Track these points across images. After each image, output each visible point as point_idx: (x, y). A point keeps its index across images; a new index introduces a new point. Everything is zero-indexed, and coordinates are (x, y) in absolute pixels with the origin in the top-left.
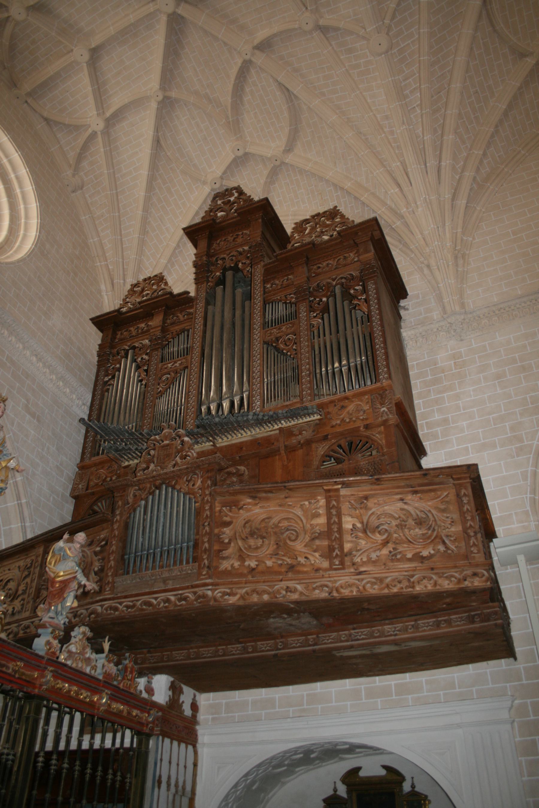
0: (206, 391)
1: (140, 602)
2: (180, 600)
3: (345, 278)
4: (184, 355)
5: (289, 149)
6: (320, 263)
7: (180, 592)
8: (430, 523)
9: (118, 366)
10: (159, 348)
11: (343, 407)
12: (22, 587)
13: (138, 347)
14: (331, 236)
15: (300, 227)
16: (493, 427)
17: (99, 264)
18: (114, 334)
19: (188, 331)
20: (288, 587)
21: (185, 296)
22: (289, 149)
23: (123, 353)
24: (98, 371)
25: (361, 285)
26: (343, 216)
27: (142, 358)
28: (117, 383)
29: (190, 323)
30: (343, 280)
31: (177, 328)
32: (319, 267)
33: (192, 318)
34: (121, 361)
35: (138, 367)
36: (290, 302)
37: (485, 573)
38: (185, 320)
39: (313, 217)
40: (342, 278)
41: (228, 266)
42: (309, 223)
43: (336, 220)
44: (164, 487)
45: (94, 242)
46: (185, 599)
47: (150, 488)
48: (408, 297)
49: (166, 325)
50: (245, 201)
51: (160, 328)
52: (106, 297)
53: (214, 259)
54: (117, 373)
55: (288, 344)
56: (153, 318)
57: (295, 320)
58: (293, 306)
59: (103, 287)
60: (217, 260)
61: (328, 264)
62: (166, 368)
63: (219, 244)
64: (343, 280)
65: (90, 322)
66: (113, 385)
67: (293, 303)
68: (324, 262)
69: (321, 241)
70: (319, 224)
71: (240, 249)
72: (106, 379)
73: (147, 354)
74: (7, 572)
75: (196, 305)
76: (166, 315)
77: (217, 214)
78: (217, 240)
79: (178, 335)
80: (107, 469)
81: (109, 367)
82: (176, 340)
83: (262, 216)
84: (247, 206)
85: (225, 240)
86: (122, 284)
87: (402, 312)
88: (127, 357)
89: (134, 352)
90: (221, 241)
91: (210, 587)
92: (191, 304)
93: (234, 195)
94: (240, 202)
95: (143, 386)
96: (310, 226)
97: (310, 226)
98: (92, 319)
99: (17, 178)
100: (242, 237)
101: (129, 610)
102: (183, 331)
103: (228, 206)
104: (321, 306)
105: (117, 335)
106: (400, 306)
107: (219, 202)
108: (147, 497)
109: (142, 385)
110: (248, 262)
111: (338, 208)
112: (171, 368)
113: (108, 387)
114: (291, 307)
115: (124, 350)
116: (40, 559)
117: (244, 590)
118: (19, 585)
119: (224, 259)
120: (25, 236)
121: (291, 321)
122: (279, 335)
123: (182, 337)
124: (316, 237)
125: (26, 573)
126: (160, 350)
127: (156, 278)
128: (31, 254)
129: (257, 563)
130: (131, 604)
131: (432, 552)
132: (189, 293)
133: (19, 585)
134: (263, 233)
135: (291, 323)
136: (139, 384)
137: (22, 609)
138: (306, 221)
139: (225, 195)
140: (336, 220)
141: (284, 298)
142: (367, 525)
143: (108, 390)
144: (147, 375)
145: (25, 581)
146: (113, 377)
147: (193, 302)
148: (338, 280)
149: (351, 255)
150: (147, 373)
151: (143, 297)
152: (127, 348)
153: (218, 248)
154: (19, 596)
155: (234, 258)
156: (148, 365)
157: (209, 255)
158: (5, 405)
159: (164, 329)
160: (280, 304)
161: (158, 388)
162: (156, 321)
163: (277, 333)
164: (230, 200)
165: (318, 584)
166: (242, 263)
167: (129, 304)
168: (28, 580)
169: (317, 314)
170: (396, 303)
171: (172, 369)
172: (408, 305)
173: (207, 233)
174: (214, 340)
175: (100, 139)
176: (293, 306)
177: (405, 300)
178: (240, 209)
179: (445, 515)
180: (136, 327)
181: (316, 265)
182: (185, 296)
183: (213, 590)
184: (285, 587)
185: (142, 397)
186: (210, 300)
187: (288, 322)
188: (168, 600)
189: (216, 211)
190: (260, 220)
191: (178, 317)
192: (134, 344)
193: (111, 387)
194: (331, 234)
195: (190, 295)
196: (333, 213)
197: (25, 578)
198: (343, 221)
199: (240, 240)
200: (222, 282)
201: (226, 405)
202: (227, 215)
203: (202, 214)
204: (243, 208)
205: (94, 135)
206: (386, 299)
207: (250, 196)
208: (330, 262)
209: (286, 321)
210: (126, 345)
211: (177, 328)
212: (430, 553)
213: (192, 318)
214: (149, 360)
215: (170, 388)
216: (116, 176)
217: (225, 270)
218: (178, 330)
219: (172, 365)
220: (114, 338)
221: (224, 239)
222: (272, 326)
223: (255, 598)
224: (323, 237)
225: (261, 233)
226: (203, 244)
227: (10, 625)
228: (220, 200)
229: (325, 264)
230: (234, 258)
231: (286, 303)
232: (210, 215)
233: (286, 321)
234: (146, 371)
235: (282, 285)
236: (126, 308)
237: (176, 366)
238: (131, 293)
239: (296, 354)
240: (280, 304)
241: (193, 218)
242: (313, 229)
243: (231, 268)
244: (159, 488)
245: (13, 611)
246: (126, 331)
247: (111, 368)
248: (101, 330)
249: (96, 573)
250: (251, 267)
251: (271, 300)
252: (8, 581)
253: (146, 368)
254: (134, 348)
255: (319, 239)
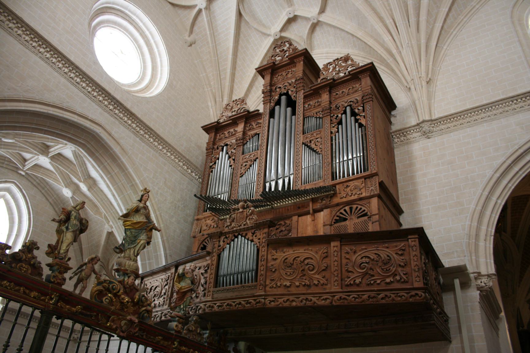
0: (269, 173)
1: (226, 304)
2: (247, 304)
3: (353, 102)
4: (256, 150)
5: (322, 11)
6: (337, 91)
7: (247, 299)
8: (392, 263)
9: (218, 156)
10: (241, 145)
11: (347, 186)
12: (164, 291)
13: (229, 145)
14: (345, 74)
15: (326, 66)
16: (446, 195)
17: (206, 90)
18: (216, 135)
19: (258, 134)
20: (307, 299)
21: (257, 112)
22: (322, 11)
23: (220, 148)
24: (207, 159)
25: (362, 107)
26: (352, 60)
27: (231, 152)
28: (218, 167)
29: (260, 130)
30: (351, 103)
31: (252, 132)
32: (337, 94)
33: (261, 126)
34: (220, 153)
35: (229, 157)
36: (319, 117)
37: (423, 294)
38: (257, 127)
39: (334, 61)
40: (351, 102)
41: (283, 92)
42: (331, 65)
43: (348, 63)
44: (240, 237)
45: (203, 76)
46: (250, 303)
47: (232, 237)
48: (397, 108)
49: (246, 130)
50: (293, 50)
51: (242, 133)
52: (211, 110)
53: (274, 88)
54: (217, 161)
55: (317, 144)
56: (238, 126)
57: (322, 129)
58: (321, 119)
59: (210, 104)
60: (276, 89)
61: (343, 92)
62: (245, 158)
63: (277, 78)
64: (351, 103)
65: (201, 129)
66: (215, 168)
67: (321, 118)
68: (340, 90)
69: (339, 77)
70: (338, 66)
71: (290, 82)
72: (211, 164)
73: (234, 149)
74: (156, 281)
75: (264, 118)
76: (246, 123)
77: (276, 58)
78: (276, 75)
79: (253, 137)
80: (211, 220)
81: (213, 157)
82: (252, 140)
83: (303, 60)
84: (294, 54)
85: (281, 75)
86: (221, 101)
87: (392, 119)
88: (223, 151)
89: (227, 148)
90: (278, 76)
91: (263, 297)
92: (260, 117)
93: (286, 46)
94: (290, 51)
95: (232, 170)
96: (332, 67)
97: (332, 67)
98: (202, 127)
99: (155, 42)
100: (291, 73)
101: (220, 308)
102: (256, 134)
103: (283, 52)
104: (338, 121)
105: (217, 136)
106: (392, 115)
107: (278, 51)
108: (230, 243)
109: (231, 168)
110: (294, 90)
111: (349, 55)
112: (248, 158)
113: (212, 169)
114: (320, 120)
115: (221, 146)
116: (173, 275)
117: (283, 299)
118: (162, 290)
119: (280, 88)
120: (161, 78)
121: (319, 130)
122: (312, 139)
123: (255, 138)
124: (335, 74)
125: (166, 283)
126: (242, 147)
127: (239, 100)
128: (165, 89)
129: (290, 283)
130: (221, 304)
131: (392, 280)
132: (258, 110)
133: (162, 290)
134: (303, 71)
135: (319, 131)
136: (230, 168)
137: (164, 303)
138: (330, 64)
139: (281, 46)
140: (348, 63)
141: (315, 114)
142: (354, 262)
143: (212, 172)
144: (234, 162)
145: (166, 287)
146: (215, 163)
147: (261, 116)
148: (348, 103)
149: (357, 85)
150: (234, 161)
151: (232, 113)
152: (223, 145)
153: (276, 81)
154: (162, 296)
155: (286, 87)
156: (235, 156)
157: (271, 85)
158: (149, 195)
159: (244, 133)
160: (313, 118)
161: (241, 171)
162: (240, 128)
163: (311, 137)
164: (284, 49)
165: (324, 297)
166: (291, 91)
167: (224, 117)
168: (167, 287)
169: (335, 125)
170: (387, 113)
171: (249, 159)
172: (397, 114)
173: (270, 71)
174: (274, 141)
175: (204, 12)
176: (321, 119)
177: (395, 111)
178: (290, 55)
179: (401, 258)
180: (228, 131)
181: (335, 92)
182: (257, 112)
183: (265, 299)
184: (305, 298)
185: (231, 177)
186: (272, 114)
187: (317, 130)
188: (240, 304)
189: (275, 57)
190: (302, 62)
191: (252, 125)
192: (227, 143)
193: (214, 170)
194: (345, 72)
195: (260, 111)
196: (346, 59)
197: (165, 286)
198: (353, 63)
199: (289, 75)
200: (278, 103)
201: (280, 182)
202: (282, 59)
203: (268, 58)
204: (292, 54)
205: (200, 11)
206: (379, 113)
207: (296, 46)
208: (344, 90)
209: (317, 130)
210: (222, 143)
211: (252, 132)
212: (390, 280)
213: (261, 126)
214: (235, 153)
215: (247, 171)
216: (215, 34)
217: (281, 95)
218: (253, 134)
219: (249, 156)
220: (215, 138)
221: (280, 74)
222: (308, 133)
223: (287, 304)
224: (340, 74)
225: (302, 71)
226: (268, 78)
227: (157, 312)
228: (278, 49)
229: (341, 92)
230: (286, 87)
231: (317, 118)
232: (272, 59)
233: (317, 130)
234: (234, 160)
235: (314, 105)
236: (223, 119)
237: (251, 157)
238: (225, 109)
239: (321, 151)
240: (313, 118)
241: (262, 62)
242: (334, 68)
243: (284, 94)
244: (237, 237)
245: (159, 305)
246: (222, 134)
247: (214, 157)
248: (208, 134)
249: (202, 286)
250: (296, 93)
251: (307, 116)
252: (156, 287)
253: (234, 158)
254: (227, 145)
255: (337, 76)
